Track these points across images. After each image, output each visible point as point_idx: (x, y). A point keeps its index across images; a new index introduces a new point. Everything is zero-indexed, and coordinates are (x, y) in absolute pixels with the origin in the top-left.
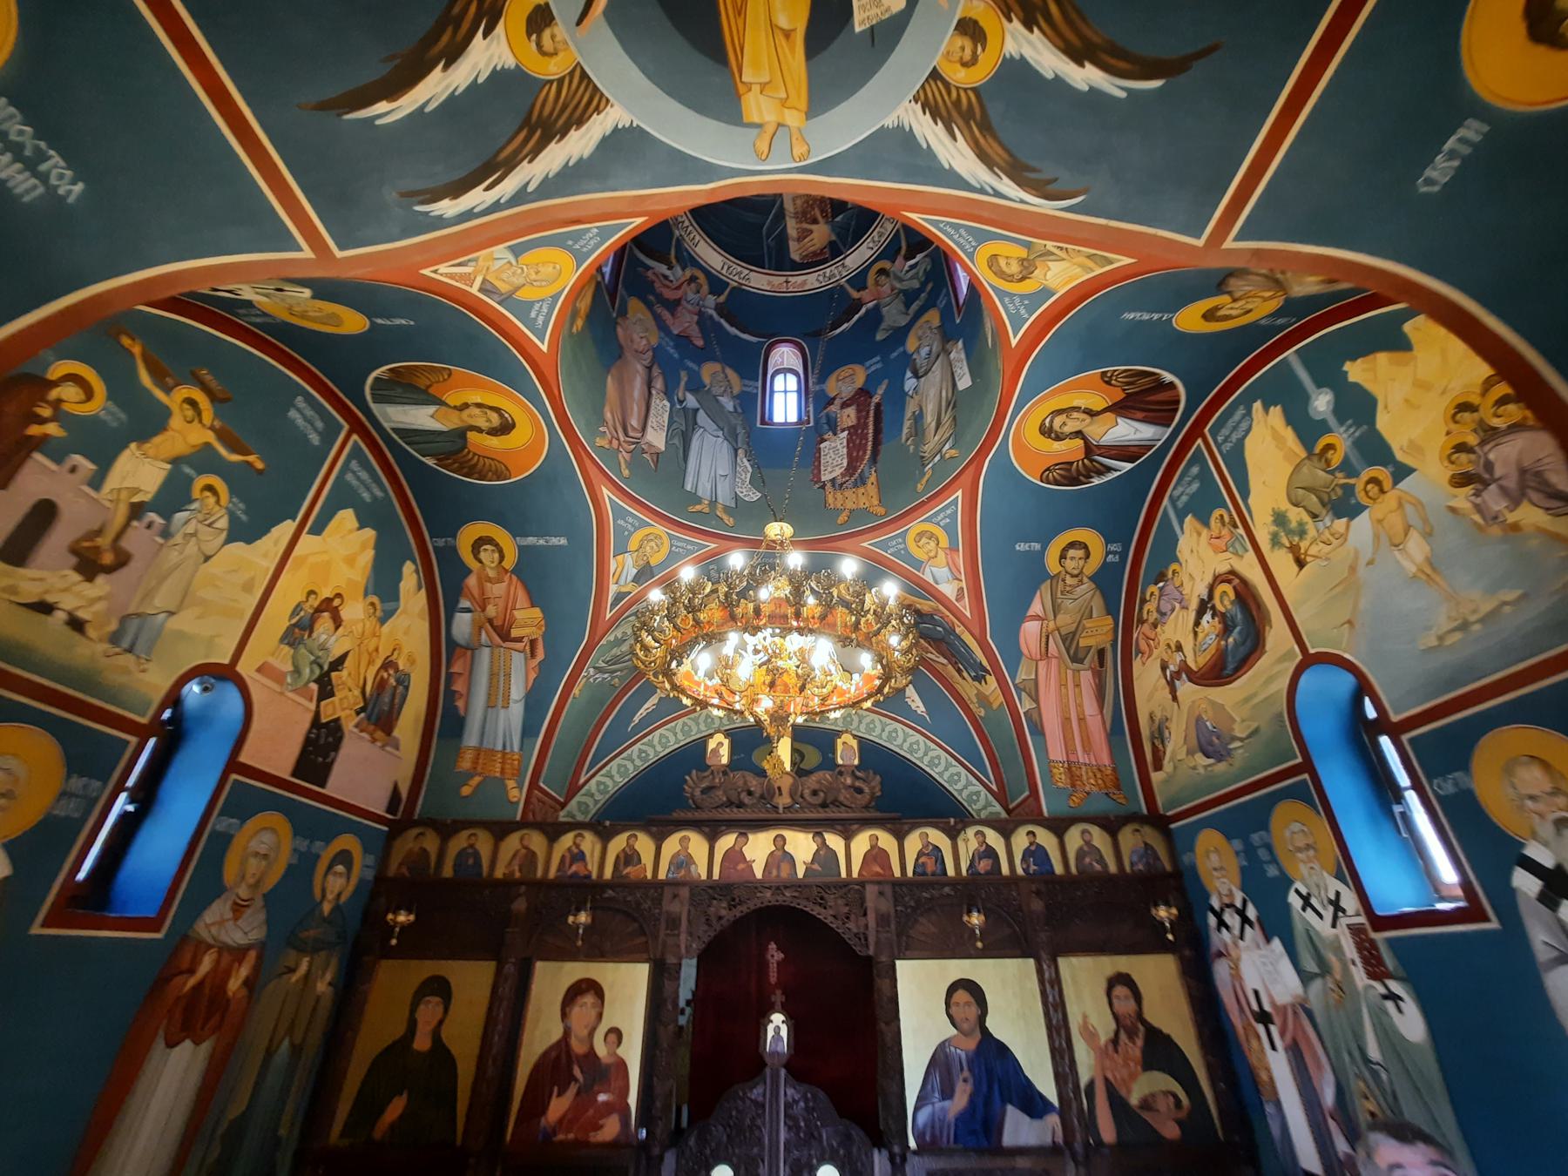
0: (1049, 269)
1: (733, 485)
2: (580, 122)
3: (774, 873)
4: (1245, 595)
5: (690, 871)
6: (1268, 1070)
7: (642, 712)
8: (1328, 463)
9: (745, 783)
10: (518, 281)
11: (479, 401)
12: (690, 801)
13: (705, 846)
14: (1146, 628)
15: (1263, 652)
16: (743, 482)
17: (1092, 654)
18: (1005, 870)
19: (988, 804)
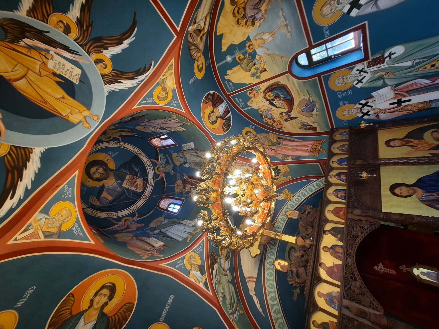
0: (168, 84)
1: (189, 226)
2: (28, 159)
3: (340, 255)
4: (270, 89)
5: (335, 297)
6: (418, 104)
7: (258, 306)
8: (242, 59)
9: (298, 257)
10: (58, 224)
11: (94, 292)
12: (302, 285)
13: (324, 285)
14: (275, 124)
15: (286, 85)
16: (190, 223)
17: (279, 140)
18: (346, 171)
19: (321, 181)
